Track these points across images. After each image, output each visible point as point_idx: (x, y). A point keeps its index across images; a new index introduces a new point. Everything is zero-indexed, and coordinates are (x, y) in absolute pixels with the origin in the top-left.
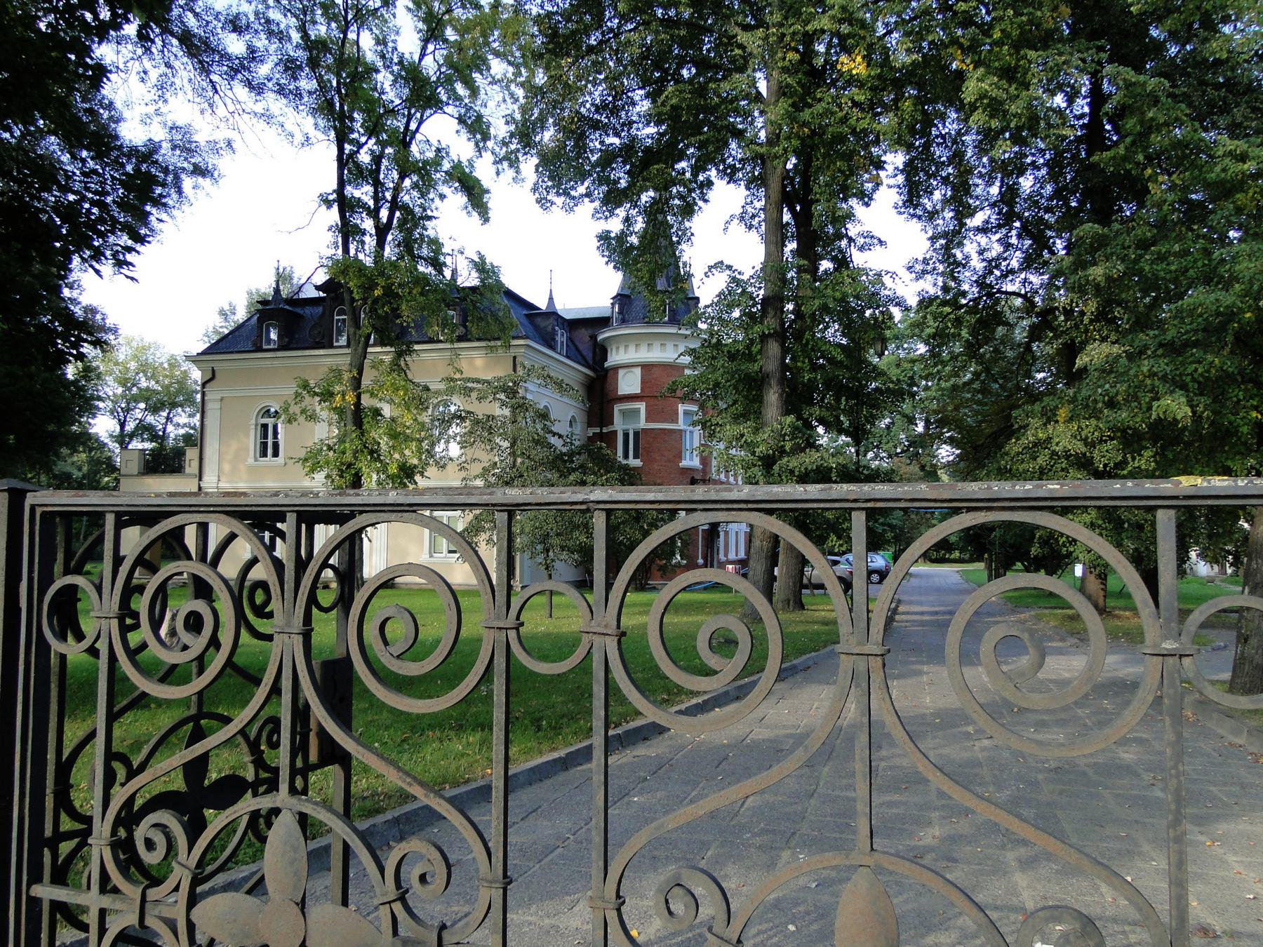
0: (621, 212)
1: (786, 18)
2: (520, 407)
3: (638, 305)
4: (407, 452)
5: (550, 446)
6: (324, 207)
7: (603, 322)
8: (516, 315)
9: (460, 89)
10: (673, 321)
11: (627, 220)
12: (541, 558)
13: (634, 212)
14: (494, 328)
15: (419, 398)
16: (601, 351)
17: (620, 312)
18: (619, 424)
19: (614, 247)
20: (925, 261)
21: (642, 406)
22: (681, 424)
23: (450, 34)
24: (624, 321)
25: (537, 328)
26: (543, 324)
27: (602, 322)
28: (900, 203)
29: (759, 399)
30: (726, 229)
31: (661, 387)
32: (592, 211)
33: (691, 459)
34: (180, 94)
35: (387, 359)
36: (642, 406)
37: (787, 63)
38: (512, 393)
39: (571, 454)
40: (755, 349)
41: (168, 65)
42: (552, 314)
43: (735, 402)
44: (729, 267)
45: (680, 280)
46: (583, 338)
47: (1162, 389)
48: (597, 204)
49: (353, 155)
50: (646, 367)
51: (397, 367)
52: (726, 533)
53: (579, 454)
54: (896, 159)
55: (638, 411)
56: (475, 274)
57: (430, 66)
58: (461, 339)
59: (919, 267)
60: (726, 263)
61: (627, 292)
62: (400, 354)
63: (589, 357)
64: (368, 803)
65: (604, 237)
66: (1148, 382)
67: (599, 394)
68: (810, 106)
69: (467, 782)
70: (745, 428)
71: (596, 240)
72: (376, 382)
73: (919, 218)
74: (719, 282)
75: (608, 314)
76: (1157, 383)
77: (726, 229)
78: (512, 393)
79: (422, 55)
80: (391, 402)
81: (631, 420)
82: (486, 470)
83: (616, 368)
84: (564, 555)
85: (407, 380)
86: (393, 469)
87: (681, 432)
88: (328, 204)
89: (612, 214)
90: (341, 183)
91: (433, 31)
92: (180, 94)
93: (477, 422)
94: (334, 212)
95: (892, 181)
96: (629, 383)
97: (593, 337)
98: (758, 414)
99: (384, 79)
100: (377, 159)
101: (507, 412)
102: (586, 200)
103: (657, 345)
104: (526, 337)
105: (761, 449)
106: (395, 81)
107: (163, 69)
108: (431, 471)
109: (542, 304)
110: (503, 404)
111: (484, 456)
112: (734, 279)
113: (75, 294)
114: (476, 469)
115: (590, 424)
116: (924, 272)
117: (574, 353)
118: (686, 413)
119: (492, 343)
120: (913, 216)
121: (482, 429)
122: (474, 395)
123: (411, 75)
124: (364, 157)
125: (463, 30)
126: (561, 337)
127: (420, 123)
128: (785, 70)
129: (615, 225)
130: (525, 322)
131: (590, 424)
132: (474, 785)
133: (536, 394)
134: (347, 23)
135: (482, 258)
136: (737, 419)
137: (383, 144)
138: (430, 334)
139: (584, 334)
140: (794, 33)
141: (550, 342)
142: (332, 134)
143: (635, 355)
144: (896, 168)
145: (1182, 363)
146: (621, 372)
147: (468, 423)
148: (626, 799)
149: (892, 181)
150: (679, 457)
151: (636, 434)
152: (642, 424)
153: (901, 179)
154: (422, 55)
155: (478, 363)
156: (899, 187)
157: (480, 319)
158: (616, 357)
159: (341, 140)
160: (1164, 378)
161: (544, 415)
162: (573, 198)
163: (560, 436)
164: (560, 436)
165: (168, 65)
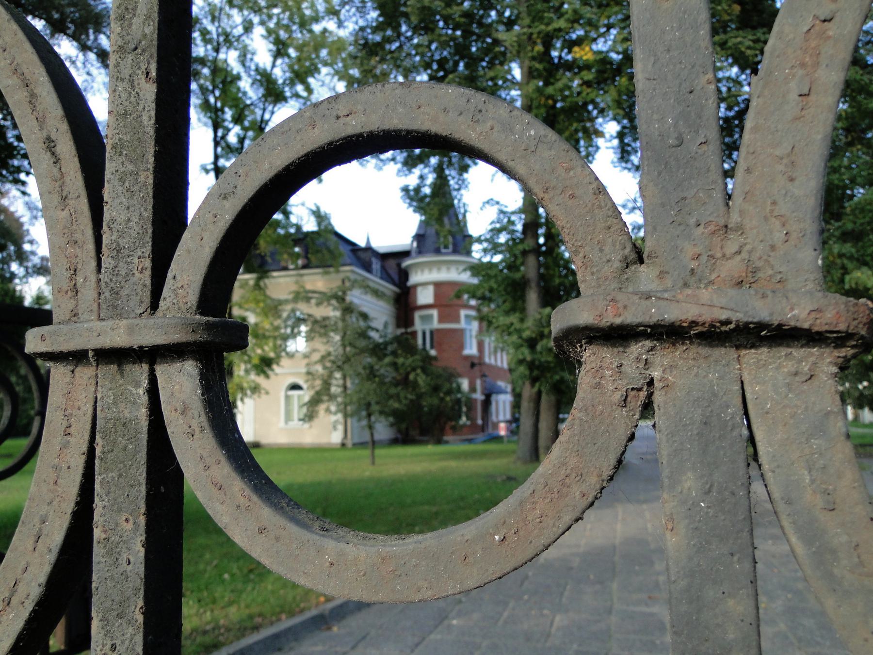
0: (417, 171)
1: (533, 21)
2: (348, 310)
3: (430, 242)
4: (266, 348)
5: (369, 338)
6: (204, 174)
7: (405, 254)
8: (344, 249)
9: (300, 88)
10: (456, 251)
11: (422, 177)
12: (364, 422)
13: (426, 171)
14: (327, 256)
15: (273, 308)
16: (404, 275)
17: (418, 246)
18: (418, 326)
19: (413, 196)
20: (635, 201)
21: (435, 313)
22: (463, 324)
23: (292, 52)
24: (420, 251)
25: (359, 259)
26: (363, 256)
27: (405, 254)
28: (616, 160)
29: (523, 298)
30: (492, 180)
31: (449, 298)
32: (396, 171)
33: (471, 348)
34: (98, 94)
35: (252, 283)
36: (435, 313)
37: (535, 53)
38: (341, 299)
39: (386, 344)
40: (519, 262)
41: (88, 74)
42: (369, 249)
43: (504, 302)
44: (498, 203)
45: (459, 226)
46: (393, 265)
47: (849, 265)
48: (399, 166)
49: (223, 137)
50: (438, 285)
51: (257, 286)
52: (497, 402)
53: (391, 343)
54: (611, 128)
55: (431, 316)
56: (313, 219)
57: (280, 73)
58: (305, 267)
59: (630, 205)
60: (496, 199)
61: (422, 232)
62: (259, 279)
63: (396, 277)
64: (208, 639)
65: (405, 190)
66: (838, 261)
67: (404, 304)
68: (553, 84)
69: (302, 611)
70: (514, 318)
71: (399, 191)
72: (242, 297)
73: (629, 170)
74: (492, 213)
75: (407, 248)
76: (845, 261)
77: (492, 180)
78: (341, 299)
79: (274, 66)
80: (254, 311)
81: (426, 323)
82: (323, 358)
83: (415, 287)
84: (382, 419)
85: (265, 295)
86: (256, 361)
87: (461, 332)
88: (207, 171)
89: (410, 171)
90: (217, 157)
91: (280, 52)
92: (98, 94)
93: (316, 322)
94: (212, 174)
95: (609, 144)
96: (425, 296)
97: (399, 265)
98: (523, 310)
99: (245, 84)
100: (241, 140)
101: (338, 314)
102: (392, 163)
103: (444, 269)
104: (350, 265)
105: (526, 334)
106: (253, 84)
107: (85, 77)
108: (285, 361)
109: (362, 244)
110: (335, 309)
111: (321, 347)
112: (502, 212)
113: (34, 248)
114: (316, 357)
115: (398, 326)
116: (634, 208)
117: (386, 275)
118: (467, 317)
119: (327, 269)
120: (625, 168)
121: (319, 327)
122: (313, 301)
123: (265, 80)
124: (232, 139)
125: (299, 49)
126: (376, 265)
127: (273, 113)
128: (533, 58)
129: (412, 180)
130: (350, 254)
131: (398, 326)
132: (308, 615)
133: (356, 297)
134: (219, 44)
135: (318, 208)
136: (507, 313)
137: (245, 129)
138: (283, 264)
139: (392, 263)
140: (539, 33)
141: (367, 267)
142: (210, 122)
143: (427, 277)
144: (611, 136)
145: (863, 247)
146: (419, 289)
147: (309, 323)
148: (446, 622)
149: (609, 144)
150: (462, 347)
151: (432, 333)
152: (436, 324)
153: (616, 142)
154: (274, 66)
155: (317, 281)
156: (613, 148)
157: (318, 251)
158: (415, 278)
159: (216, 126)
160: (851, 258)
161: (365, 316)
162: (382, 160)
163: (377, 331)
164: (377, 331)
165: (88, 74)
